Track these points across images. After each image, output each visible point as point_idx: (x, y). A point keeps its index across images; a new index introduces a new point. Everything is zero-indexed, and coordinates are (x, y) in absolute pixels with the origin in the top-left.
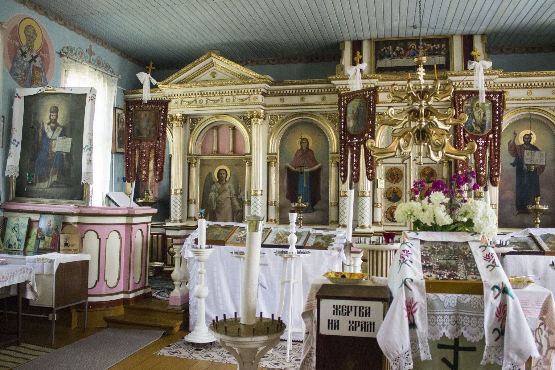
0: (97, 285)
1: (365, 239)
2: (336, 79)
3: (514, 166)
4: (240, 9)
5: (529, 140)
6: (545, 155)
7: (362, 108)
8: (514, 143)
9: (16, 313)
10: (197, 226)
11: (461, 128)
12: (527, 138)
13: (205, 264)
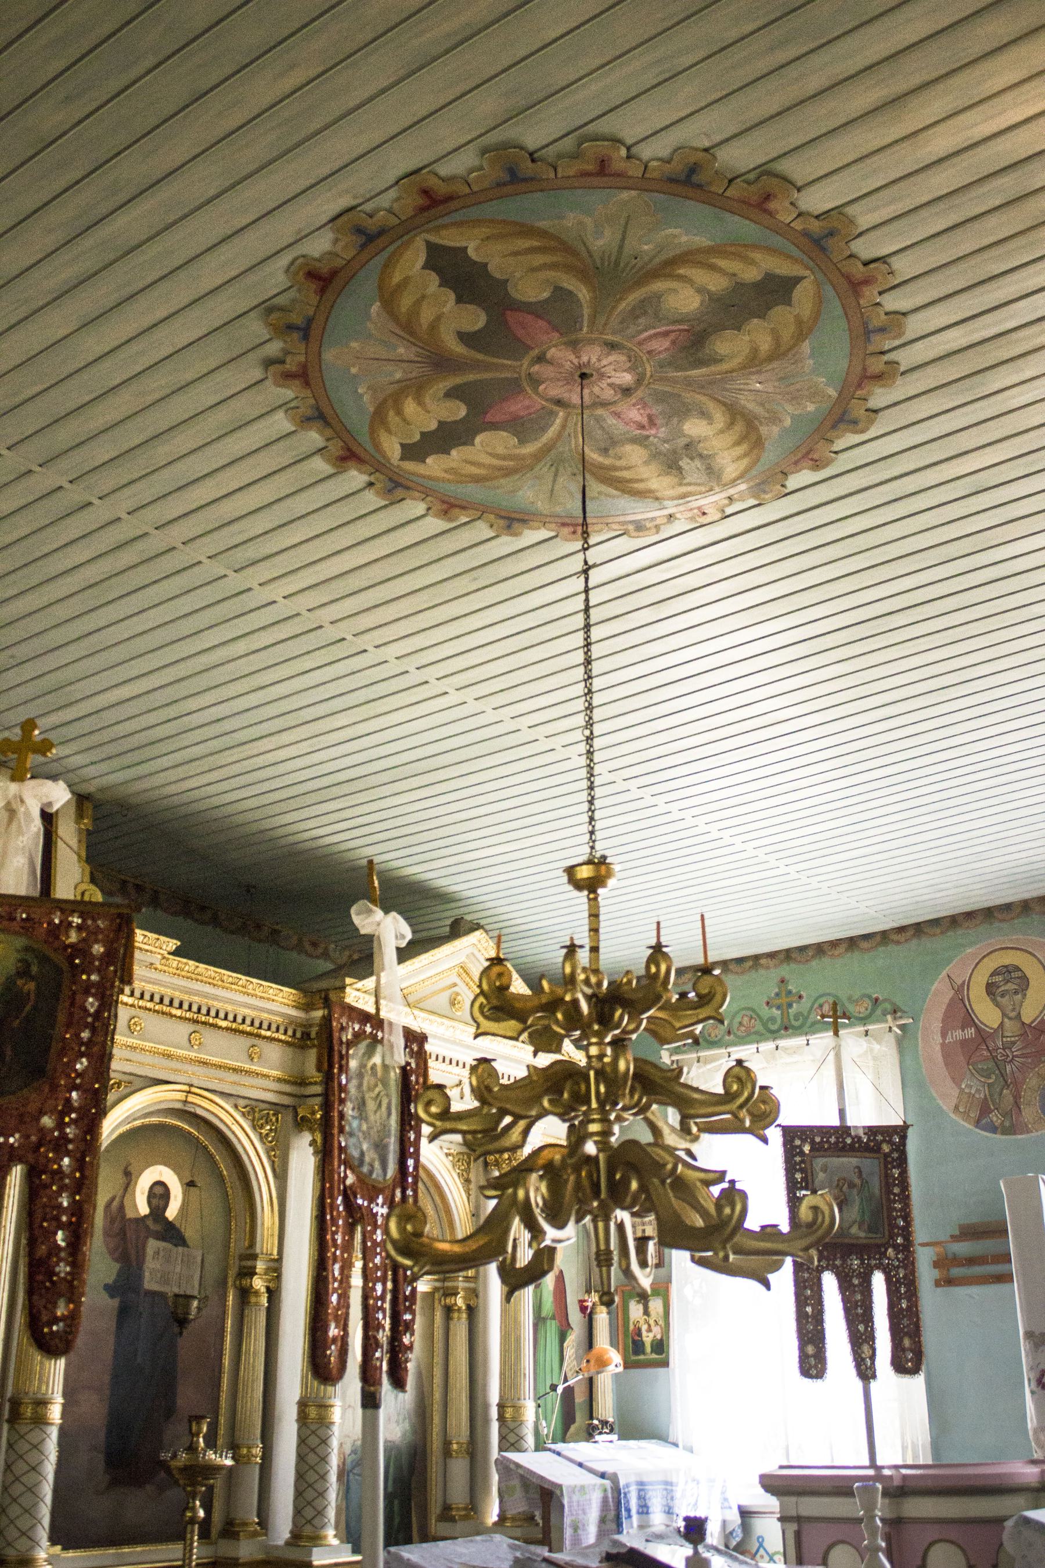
0: (825, 1548)
1: (923, 1245)
2: (118, 906)
3: (112, 1296)
4: (251, 761)
5: (162, 1203)
6: (199, 1258)
7: (31, 986)
8: (122, 1207)
9: (516, 375)
10: (992, 975)
11: (185, 1102)
12: (159, 1194)
13: (888, 1281)
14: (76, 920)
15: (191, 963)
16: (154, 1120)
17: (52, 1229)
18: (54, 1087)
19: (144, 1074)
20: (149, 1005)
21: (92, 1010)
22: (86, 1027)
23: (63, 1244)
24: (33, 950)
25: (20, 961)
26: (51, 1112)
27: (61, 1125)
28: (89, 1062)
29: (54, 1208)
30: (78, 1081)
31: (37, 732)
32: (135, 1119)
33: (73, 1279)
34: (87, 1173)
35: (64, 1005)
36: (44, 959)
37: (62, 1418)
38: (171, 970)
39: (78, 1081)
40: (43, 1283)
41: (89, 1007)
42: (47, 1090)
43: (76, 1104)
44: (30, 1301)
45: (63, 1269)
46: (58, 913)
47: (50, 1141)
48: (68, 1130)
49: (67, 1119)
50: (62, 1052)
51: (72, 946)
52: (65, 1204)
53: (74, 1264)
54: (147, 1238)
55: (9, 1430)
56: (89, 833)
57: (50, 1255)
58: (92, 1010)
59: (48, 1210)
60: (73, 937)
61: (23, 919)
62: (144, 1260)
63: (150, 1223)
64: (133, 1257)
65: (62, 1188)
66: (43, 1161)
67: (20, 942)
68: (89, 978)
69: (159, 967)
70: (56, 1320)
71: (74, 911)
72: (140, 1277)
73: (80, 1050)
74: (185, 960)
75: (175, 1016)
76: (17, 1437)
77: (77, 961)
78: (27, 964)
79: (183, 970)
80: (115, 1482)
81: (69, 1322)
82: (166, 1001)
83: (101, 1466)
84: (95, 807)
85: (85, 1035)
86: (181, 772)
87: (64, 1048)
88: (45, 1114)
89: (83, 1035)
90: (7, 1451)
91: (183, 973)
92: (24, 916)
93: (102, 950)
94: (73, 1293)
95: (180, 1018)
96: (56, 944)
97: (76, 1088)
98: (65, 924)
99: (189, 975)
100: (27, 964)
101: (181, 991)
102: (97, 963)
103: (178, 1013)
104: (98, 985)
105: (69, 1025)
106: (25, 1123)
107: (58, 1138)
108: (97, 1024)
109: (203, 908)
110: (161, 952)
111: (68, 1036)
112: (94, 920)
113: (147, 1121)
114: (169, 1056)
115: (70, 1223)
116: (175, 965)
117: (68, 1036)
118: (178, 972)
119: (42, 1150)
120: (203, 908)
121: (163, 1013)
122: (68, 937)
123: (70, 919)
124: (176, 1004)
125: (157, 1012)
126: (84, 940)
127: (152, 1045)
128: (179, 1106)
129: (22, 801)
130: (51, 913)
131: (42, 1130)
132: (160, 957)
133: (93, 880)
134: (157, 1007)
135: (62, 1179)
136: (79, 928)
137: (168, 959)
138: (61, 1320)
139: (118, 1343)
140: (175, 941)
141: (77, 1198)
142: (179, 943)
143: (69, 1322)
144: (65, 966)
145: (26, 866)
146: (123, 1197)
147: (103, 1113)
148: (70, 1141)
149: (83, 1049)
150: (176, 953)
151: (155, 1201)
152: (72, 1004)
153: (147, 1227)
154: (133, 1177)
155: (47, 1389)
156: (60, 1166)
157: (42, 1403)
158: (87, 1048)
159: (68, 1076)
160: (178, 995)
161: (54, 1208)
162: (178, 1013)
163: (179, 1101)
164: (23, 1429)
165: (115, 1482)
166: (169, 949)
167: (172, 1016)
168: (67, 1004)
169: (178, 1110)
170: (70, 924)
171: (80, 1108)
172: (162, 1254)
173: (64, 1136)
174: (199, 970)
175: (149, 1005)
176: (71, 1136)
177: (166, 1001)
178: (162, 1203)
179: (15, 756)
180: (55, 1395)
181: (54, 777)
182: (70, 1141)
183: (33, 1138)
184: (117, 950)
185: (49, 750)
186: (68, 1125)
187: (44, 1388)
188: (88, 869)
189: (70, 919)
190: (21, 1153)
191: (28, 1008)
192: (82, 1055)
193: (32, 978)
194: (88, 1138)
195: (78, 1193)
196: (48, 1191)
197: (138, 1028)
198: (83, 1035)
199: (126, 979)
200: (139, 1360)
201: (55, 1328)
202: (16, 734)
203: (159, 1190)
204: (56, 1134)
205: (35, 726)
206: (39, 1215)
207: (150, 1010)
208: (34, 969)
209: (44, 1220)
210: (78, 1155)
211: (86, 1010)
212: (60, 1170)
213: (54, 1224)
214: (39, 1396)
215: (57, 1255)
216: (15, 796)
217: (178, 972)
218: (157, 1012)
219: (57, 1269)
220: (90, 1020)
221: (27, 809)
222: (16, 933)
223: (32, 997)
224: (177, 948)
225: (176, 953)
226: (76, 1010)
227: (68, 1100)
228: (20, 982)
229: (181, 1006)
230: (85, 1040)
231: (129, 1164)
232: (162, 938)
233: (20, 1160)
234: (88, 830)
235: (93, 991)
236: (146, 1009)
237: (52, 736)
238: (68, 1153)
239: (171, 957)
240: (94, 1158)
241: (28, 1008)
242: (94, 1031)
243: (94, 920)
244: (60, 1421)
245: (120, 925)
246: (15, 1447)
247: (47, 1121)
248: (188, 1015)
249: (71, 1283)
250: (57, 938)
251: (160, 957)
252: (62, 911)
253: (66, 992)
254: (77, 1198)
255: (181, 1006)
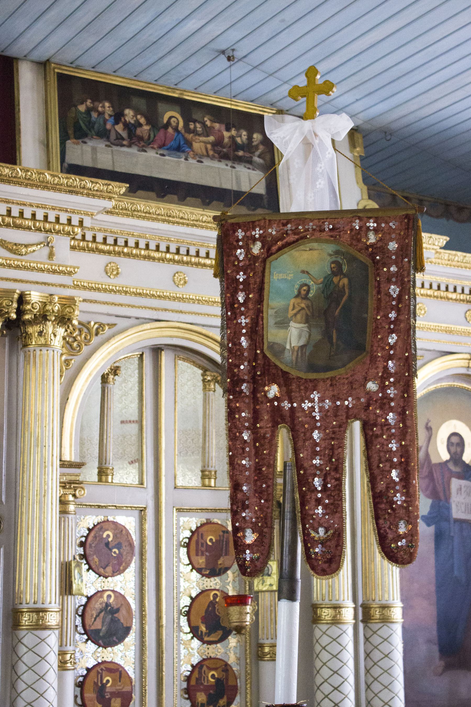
3: (429, 525)
5: (459, 450)
14: (372, 224)
15: (459, 253)
16: (445, 384)
17: (387, 468)
18: (373, 359)
19: (432, 348)
20: (430, 292)
21: (395, 296)
22: (392, 309)
23: (397, 480)
24: (343, 254)
25: (333, 262)
26: (374, 379)
27: (383, 388)
28: (398, 337)
29: (386, 452)
30: (392, 352)
31: (318, 77)
32: (429, 385)
33: (408, 506)
34: (408, 423)
35: (372, 291)
36: (352, 259)
37: (403, 618)
38: (444, 262)
39: (392, 352)
40: (386, 510)
41: (392, 293)
42: (368, 362)
43: (393, 371)
44: (377, 524)
45: (399, 498)
46: (357, 221)
47: (376, 401)
48: (389, 391)
49: (387, 383)
50: (376, 331)
51: (372, 245)
52: (394, 449)
53: (407, 494)
54: (450, 478)
55: (364, 628)
56: (362, 159)
57: (388, 488)
58: (395, 296)
59: (382, 454)
60: (372, 238)
61: (330, 230)
62: (450, 493)
63: (451, 466)
64: (441, 495)
65: (391, 437)
66: (372, 417)
67: (330, 248)
68: (389, 270)
69: (434, 260)
70: (400, 537)
71: (370, 218)
72: (449, 509)
73: (389, 328)
74: (454, 252)
75: (451, 299)
76: (371, 633)
77: (378, 257)
78: (339, 265)
79: (453, 261)
80: (448, 667)
81: (409, 538)
82: (443, 288)
83: (437, 654)
84: (364, 137)
85: (393, 315)
86: (425, 99)
87: (377, 327)
88: (369, 380)
89: (390, 315)
90: (365, 644)
91: (454, 263)
92: (331, 227)
93: (396, 246)
94: (409, 517)
95: (456, 300)
96: (360, 245)
97: (391, 358)
98: (364, 229)
99: (459, 264)
100: (339, 265)
101: (453, 278)
102: (394, 257)
103: (454, 296)
104: (396, 274)
105: (378, 309)
106: (355, 389)
107: (382, 398)
108: (400, 306)
109: (461, 209)
110: (435, 247)
111: (379, 317)
112: (387, 223)
113: (439, 385)
114: (450, 332)
115: (401, 463)
116: (446, 257)
117: (379, 317)
118: (449, 262)
119: (371, 408)
120: (461, 209)
121: (441, 298)
122: (368, 239)
123: (368, 224)
124: (451, 289)
125: (437, 297)
126: (381, 240)
127: (435, 324)
128: (464, 371)
129: (316, 135)
130: (352, 222)
131: (368, 393)
132: (434, 251)
133: (370, 197)
134: (436, 294)
135: (389, 429)
136: (376, 230)
137: (440, 253)
138: (403, 538)
139: (437, 560)
140: (445, 237)
141: (403, 443)
142: (448, 239)
143: (409, 538)
144: (368, 261)
145: (327, 186)
146: (428, 446)
147: (413, 374)
148: (392, 400)
149: (392, 326)
150: (446, 247)
151: (453, 449)
152: (379, 292)
153: (449, 470)
154: (433, 432)
155: (389, 597)
156: (387, 420)
157: (385, 607)
158: (395, 326)
159: (383, 349)
160: (452, 282)
161: (386, 452)
162: (454, 296)
163: (462, 367)
164: (375, 627)
165: (448, 667)
166: (440, 244)
167: (448, 299)
168: (374, 292)
169: (462, 374)
170: (368, 228)
171: (396, 373)
172: (463, 490)
173: (386, 397)
174: (467, 258)
175: (430, 292)
176: (392, 396)
177: (443, 288)
178: (459, 450)
179: (305, 99)
180: (395, 601)
181: (337, 111)
182: (392, 400)
183: (363, 400)
184: (408, 245)
185: (331, 89)
186: (389, 388)
187: (386, 596)
188: (365, 188)
189: (368, 224)
190: (356, 411)
191: (345, 298)
192: (392, 332)
193: (345, 276)
194: (406, 396)
195: (404, 440)
196: (380, 439)
197: (423, 312)
198: (390, 315)
199: (419, 267)
200: (456, 573)
201: (399, 544)
202: (302, 81)
203: (455, 440)
204: (380, 395)
205: (316, 72)
206: (375, 458)
207: (430, 296)
208: (345, 269)
209: (380, 462)
210: (400, 410)
211: (390, 296)
212: (387, 423)
213: (388, 464)
214: (384, 602)
215: (394, 488)
216: (310, 131)
217: (449, 262)
218: (437, 297)
219: (395, 499)
220: (394, 303)
221: (321, 140)
222: (327, 241)
223: (347, 291)
224: (447, 243)
225: (446, 247)
226: (382, 296)
227: (386, 368)
228: (335, 280)
229: (455, 290)
230: (393, 319)
231: (429, 421)
232: (434, 236)
233: (356, 418)
234: (360, 156)
235: (394, 280)
236: (427, 295)
237: (332, 78)
238: (391, 409)
239: (442, 251)
240: (412, 409)
241: (345, 298)
242: (399, 311)
243: (387, 223)
244: (402, 620)
245: (408, 224)
246: (370, 640)
247: (372, 386)
248: (462, 297)
249: (407, 509)
250: (359, 240)
251: (434, 251)
252: (360, 218)
253: (372, 283)
254: (403, 443)
255: (455, 290)
